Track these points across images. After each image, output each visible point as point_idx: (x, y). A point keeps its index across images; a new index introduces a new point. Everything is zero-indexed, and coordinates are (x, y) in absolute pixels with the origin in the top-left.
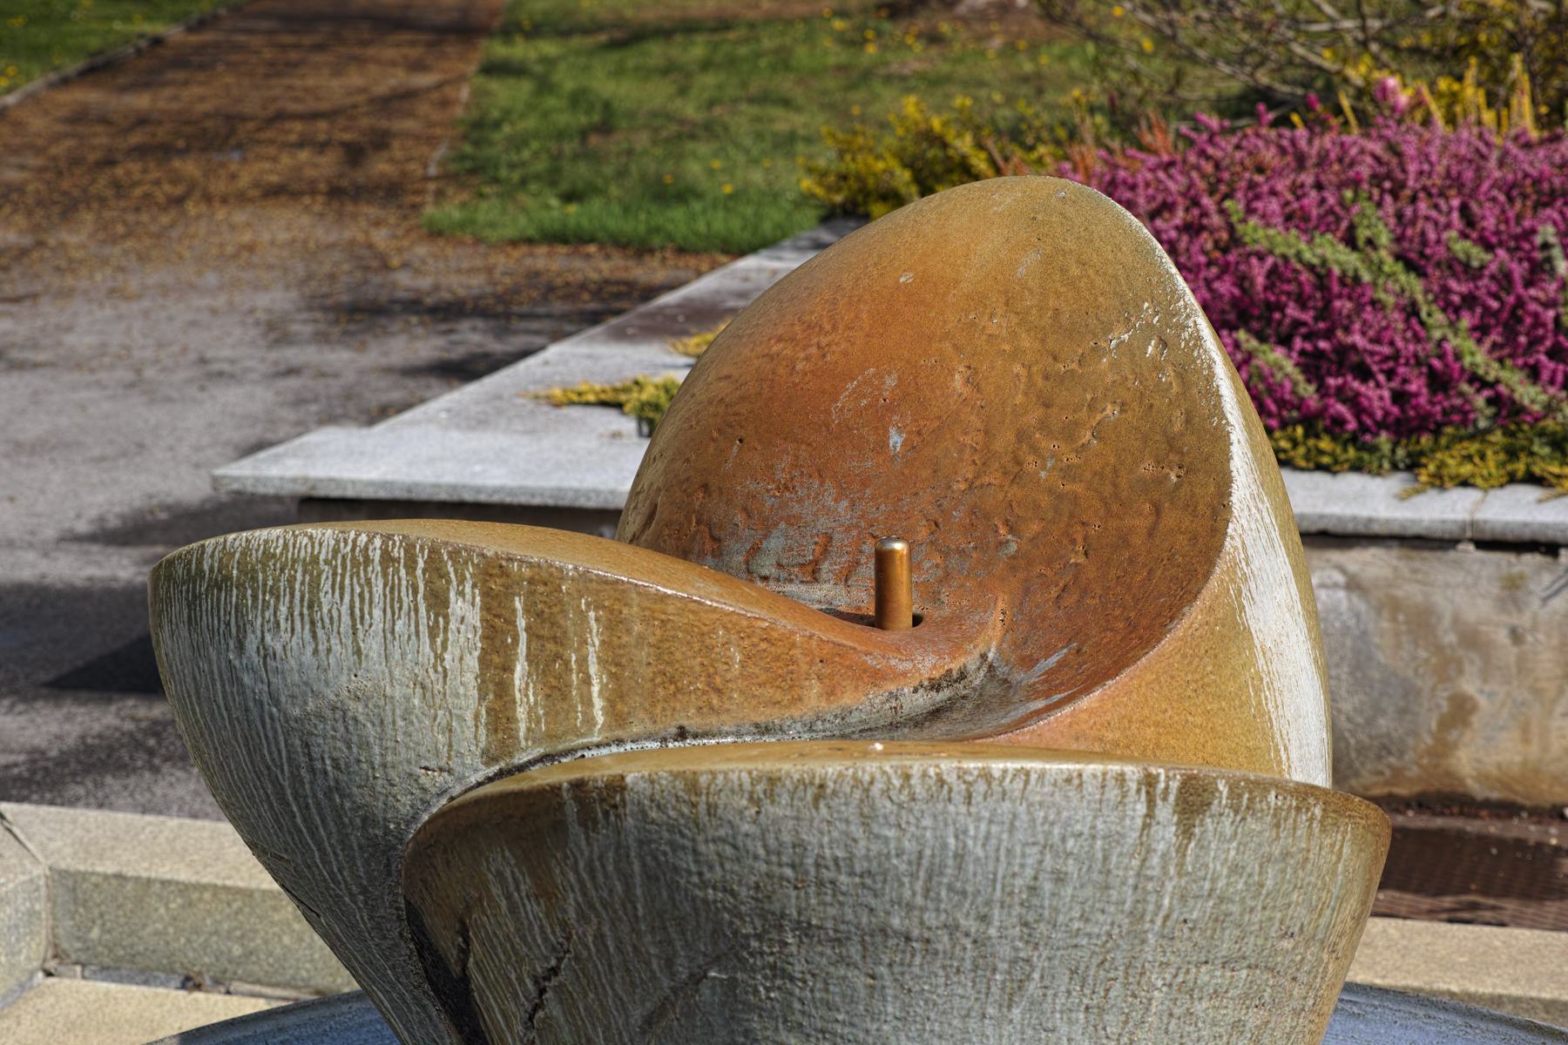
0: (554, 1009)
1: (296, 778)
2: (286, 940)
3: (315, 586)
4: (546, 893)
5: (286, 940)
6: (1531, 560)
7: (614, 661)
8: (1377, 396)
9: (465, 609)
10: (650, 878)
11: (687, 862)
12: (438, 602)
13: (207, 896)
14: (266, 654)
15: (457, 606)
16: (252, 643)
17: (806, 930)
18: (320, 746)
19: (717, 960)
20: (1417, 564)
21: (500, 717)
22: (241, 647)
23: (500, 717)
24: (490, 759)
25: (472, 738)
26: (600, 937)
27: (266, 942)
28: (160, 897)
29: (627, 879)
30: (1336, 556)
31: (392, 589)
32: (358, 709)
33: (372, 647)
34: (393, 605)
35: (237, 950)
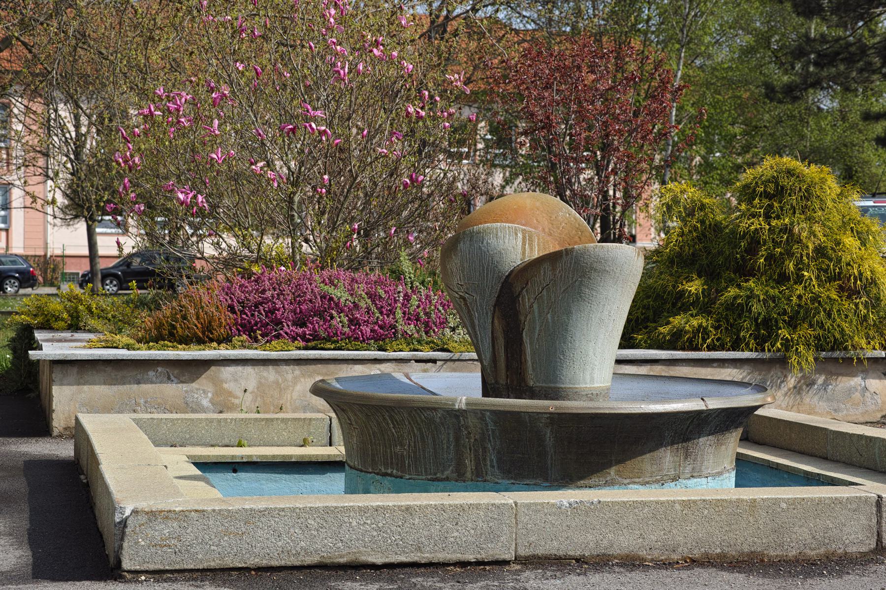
0: (545, 292)
1: (488, 265)
2: (203, 432)
3: (497, 232)
4: (554, 270)
5: (203, 432)
6: (430, 364)
7: (538, 245)
8: (367, 330)
9: (520, 235)
10: (575, 263)
11: (582, 259)
12: (516, 234)
13: (179, 422)
14: (488, 243)
15: (519, 235)
16: (485, 242)
17: (595, 270)
18: (495, 259)
19: (580, 277)
20: (400, 367)
21: (524, 253)
22: (482, 243)
23: (524, 253)
24: (521, 260)
25: (519, 256)
26: (561, 276)
27: (197, 433)
28: (165, 423)
29: (571, 263)
30: (378, 366)
31: (509, 232)
32: (503, 251)
33: (507, 241)
34: (510, 236)
35: (188, 436)
